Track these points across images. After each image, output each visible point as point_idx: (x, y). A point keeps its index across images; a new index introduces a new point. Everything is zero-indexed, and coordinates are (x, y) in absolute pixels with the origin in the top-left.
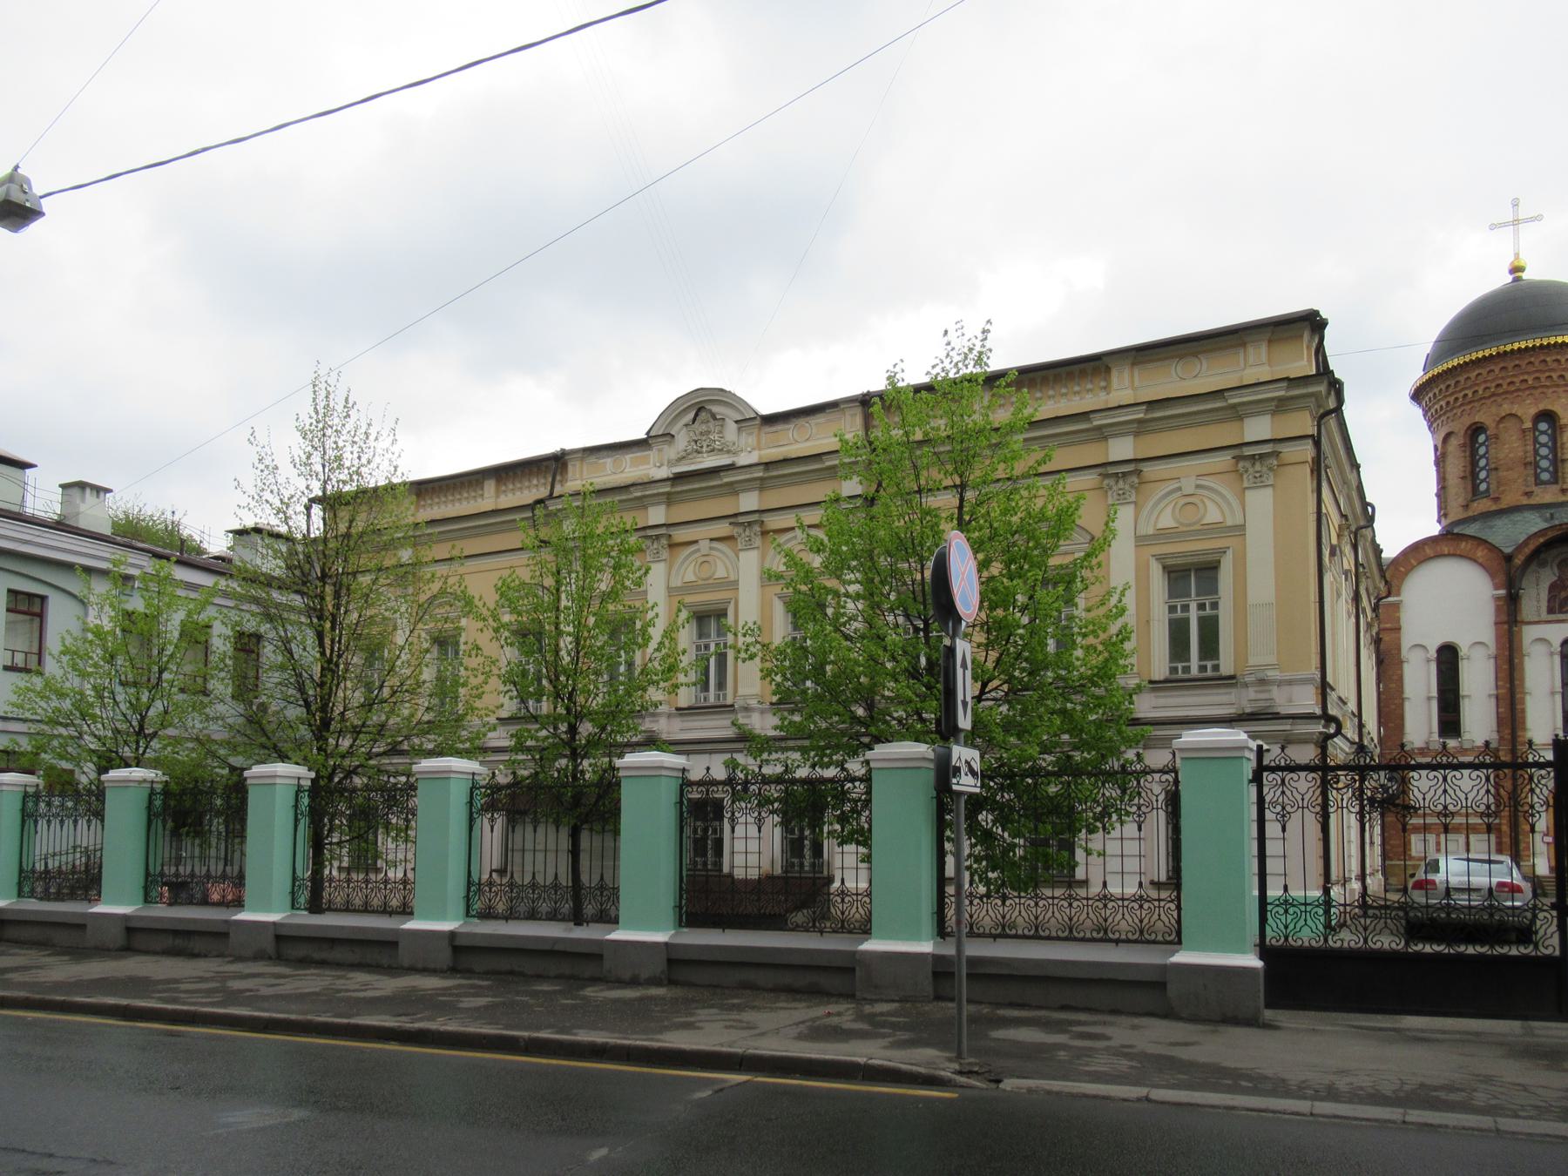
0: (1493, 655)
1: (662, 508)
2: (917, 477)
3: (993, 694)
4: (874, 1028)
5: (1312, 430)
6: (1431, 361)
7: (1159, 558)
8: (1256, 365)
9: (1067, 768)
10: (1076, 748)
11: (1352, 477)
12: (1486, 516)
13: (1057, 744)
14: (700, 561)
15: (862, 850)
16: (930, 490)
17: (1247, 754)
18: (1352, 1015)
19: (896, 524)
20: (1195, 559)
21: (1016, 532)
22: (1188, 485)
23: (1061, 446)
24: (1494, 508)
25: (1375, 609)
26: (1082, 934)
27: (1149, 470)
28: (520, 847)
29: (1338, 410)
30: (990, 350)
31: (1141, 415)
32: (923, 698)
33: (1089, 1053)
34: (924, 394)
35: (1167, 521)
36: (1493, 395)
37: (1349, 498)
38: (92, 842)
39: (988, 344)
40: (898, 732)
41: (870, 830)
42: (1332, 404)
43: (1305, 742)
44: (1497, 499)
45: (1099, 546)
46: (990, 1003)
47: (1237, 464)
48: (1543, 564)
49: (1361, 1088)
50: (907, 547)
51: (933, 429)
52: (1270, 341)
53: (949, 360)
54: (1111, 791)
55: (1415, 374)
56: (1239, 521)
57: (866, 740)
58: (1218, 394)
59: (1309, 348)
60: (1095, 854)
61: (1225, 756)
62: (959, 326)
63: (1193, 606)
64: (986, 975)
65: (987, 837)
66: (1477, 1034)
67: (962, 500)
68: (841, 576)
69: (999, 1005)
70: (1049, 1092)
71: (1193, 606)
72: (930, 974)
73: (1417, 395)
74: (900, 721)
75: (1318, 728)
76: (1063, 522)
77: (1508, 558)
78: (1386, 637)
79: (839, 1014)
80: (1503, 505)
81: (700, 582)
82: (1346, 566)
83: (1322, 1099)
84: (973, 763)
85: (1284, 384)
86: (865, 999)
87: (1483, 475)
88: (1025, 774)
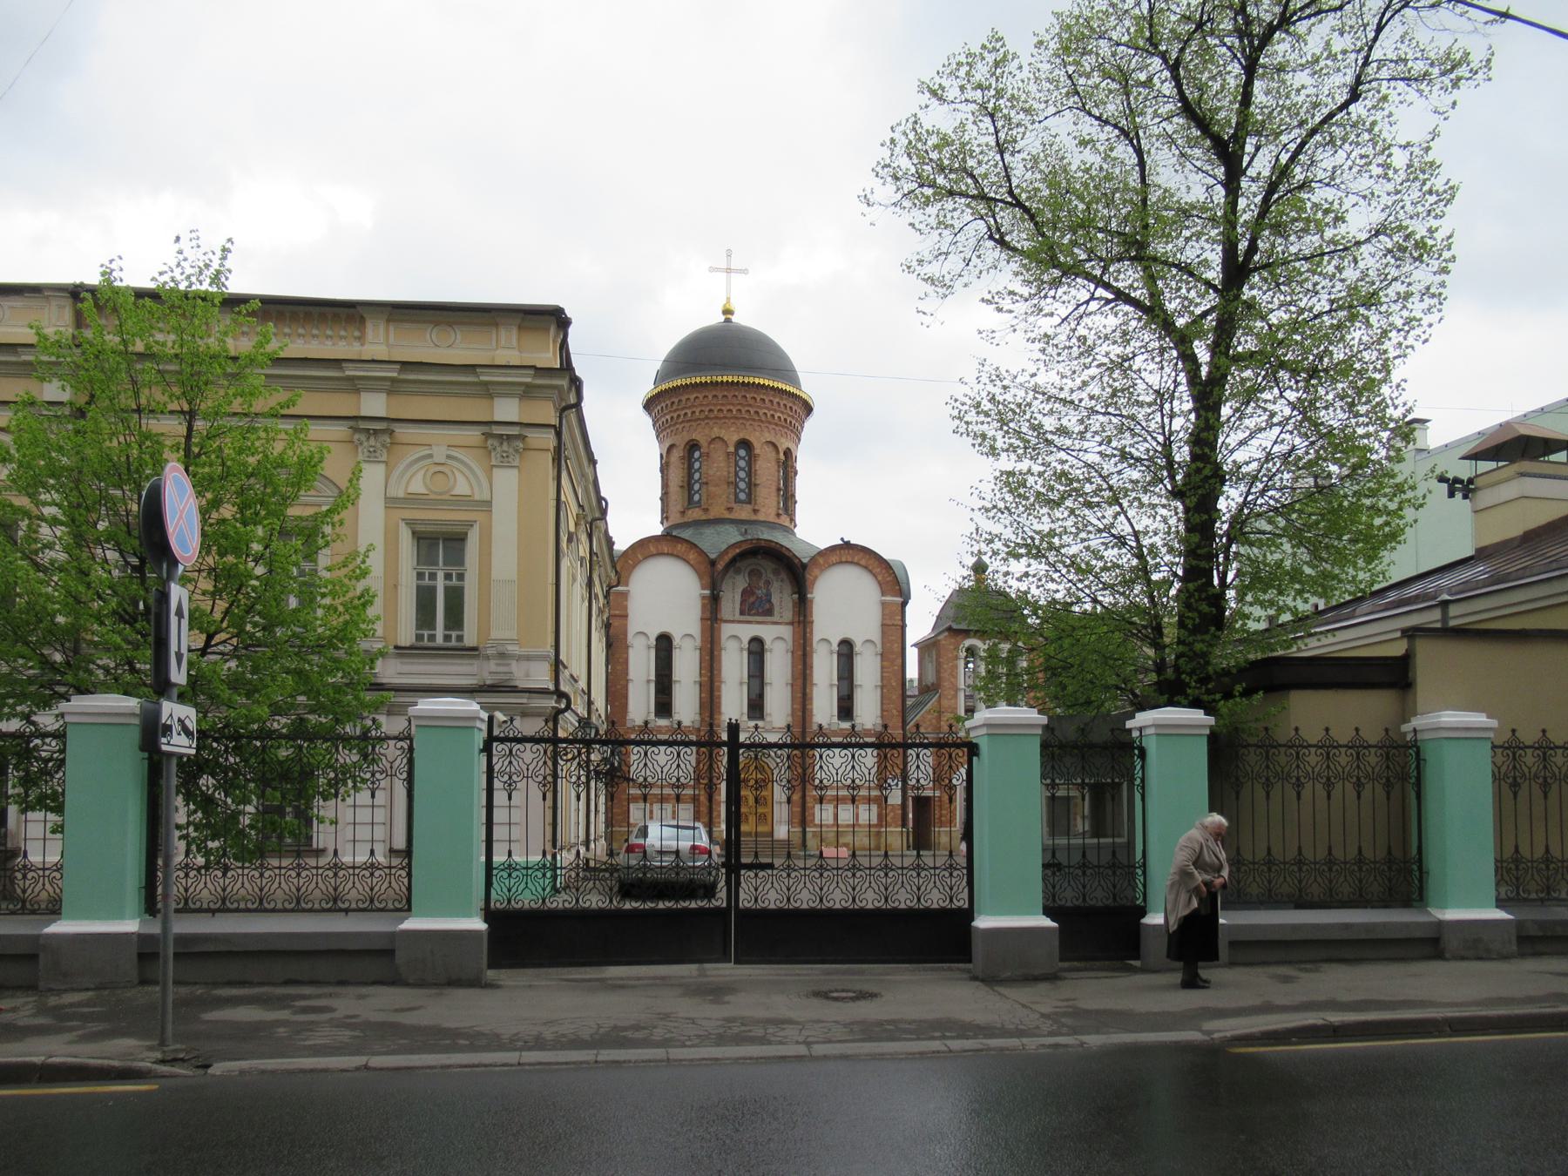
0: (109, 282)
1: (383, 397)
2: (137, 395)
3: (221, 648)
4: (61, 1020)
5: (554, 421)
6: (661, 377)
7: (410, 523)
8: (507, 348)
9: (299, 731)
10: (312, 711)
11: (589, 471)
12: (697, 524)
13: (293, 706)
14: (432, 471)
15: (51, 817)
16: (152, 411)
17: (478, 724)
18: (566, 970)
19: (107, 443)
20: (444, 529)
21: (252, 475)
22: (440, 453)
23: (308, 389)
24: (704, 518)
25: (607, 596)
26: (310, 905)
27: (403, 432)
29: (577, 406)
30: (230, 271)
31: (395, 375)
32: (136, 646)
33: (310, 1027)
34: (148, 302)
35: (417, 486)
36: (707, 418)
37: (586, 490)
39: (228, 264)
40: (103, 683)
41: (63, 794)
42: (573, 400)
43: (539, 715)
44: (706, 510)
45: (346, 498)
46: (206, 984)
47: (486, 440)
48: (738, 571)
49: (564, 1035)
50: (126, 473)
51: (157, 342)
52: (520, 328)
53: (179, 270)
54: (349, 757)
55: (647, 387)
56: (486, 497)
57: (62, 689)
58: (471, 368)
59: (554, 342)
60: (327, 821)
61: (457, 725)
62: (194, 235)
63: (440, 575)
64: (193, 952)
65: (207, 803)
66: (663, 978)
67: (190, 429)
68: (34, 494)
69: (216, 985)
70: (263, 1072)
71: (440, 575)
72: (135, 957)
73: (649, 405)
74: (107, 670)
75: (551, 703)
76: (306, 470)
77: (713, 563)
78: (615, 623)
79: (14, 1010)
80: (711, 516)
81: (432, 497)
82: (582, 553)
83: (530, 1049)
84: (187, 722)
85: (532, 372)
86: (50, 990)
87: (697, 487)
88: (252, 736)
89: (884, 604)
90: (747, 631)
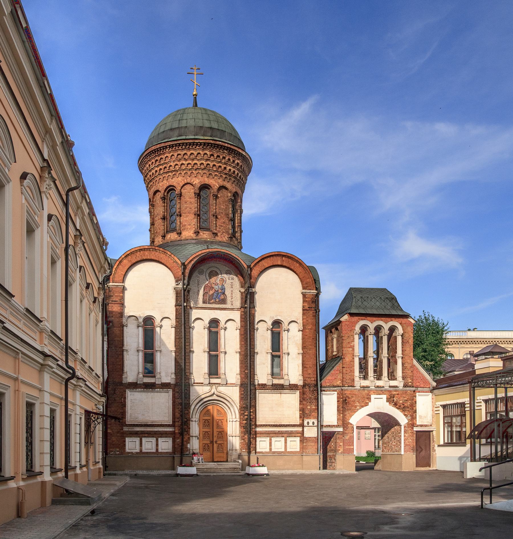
0: (174, 326)
28: (224, 372)
38: (458, 333)
48: (201, 273)
89: (304, 295)
90: (208, 315)
